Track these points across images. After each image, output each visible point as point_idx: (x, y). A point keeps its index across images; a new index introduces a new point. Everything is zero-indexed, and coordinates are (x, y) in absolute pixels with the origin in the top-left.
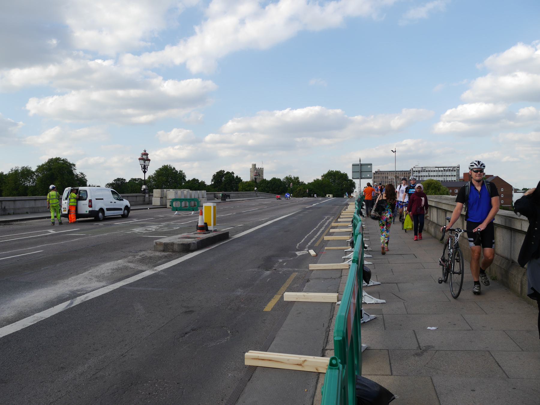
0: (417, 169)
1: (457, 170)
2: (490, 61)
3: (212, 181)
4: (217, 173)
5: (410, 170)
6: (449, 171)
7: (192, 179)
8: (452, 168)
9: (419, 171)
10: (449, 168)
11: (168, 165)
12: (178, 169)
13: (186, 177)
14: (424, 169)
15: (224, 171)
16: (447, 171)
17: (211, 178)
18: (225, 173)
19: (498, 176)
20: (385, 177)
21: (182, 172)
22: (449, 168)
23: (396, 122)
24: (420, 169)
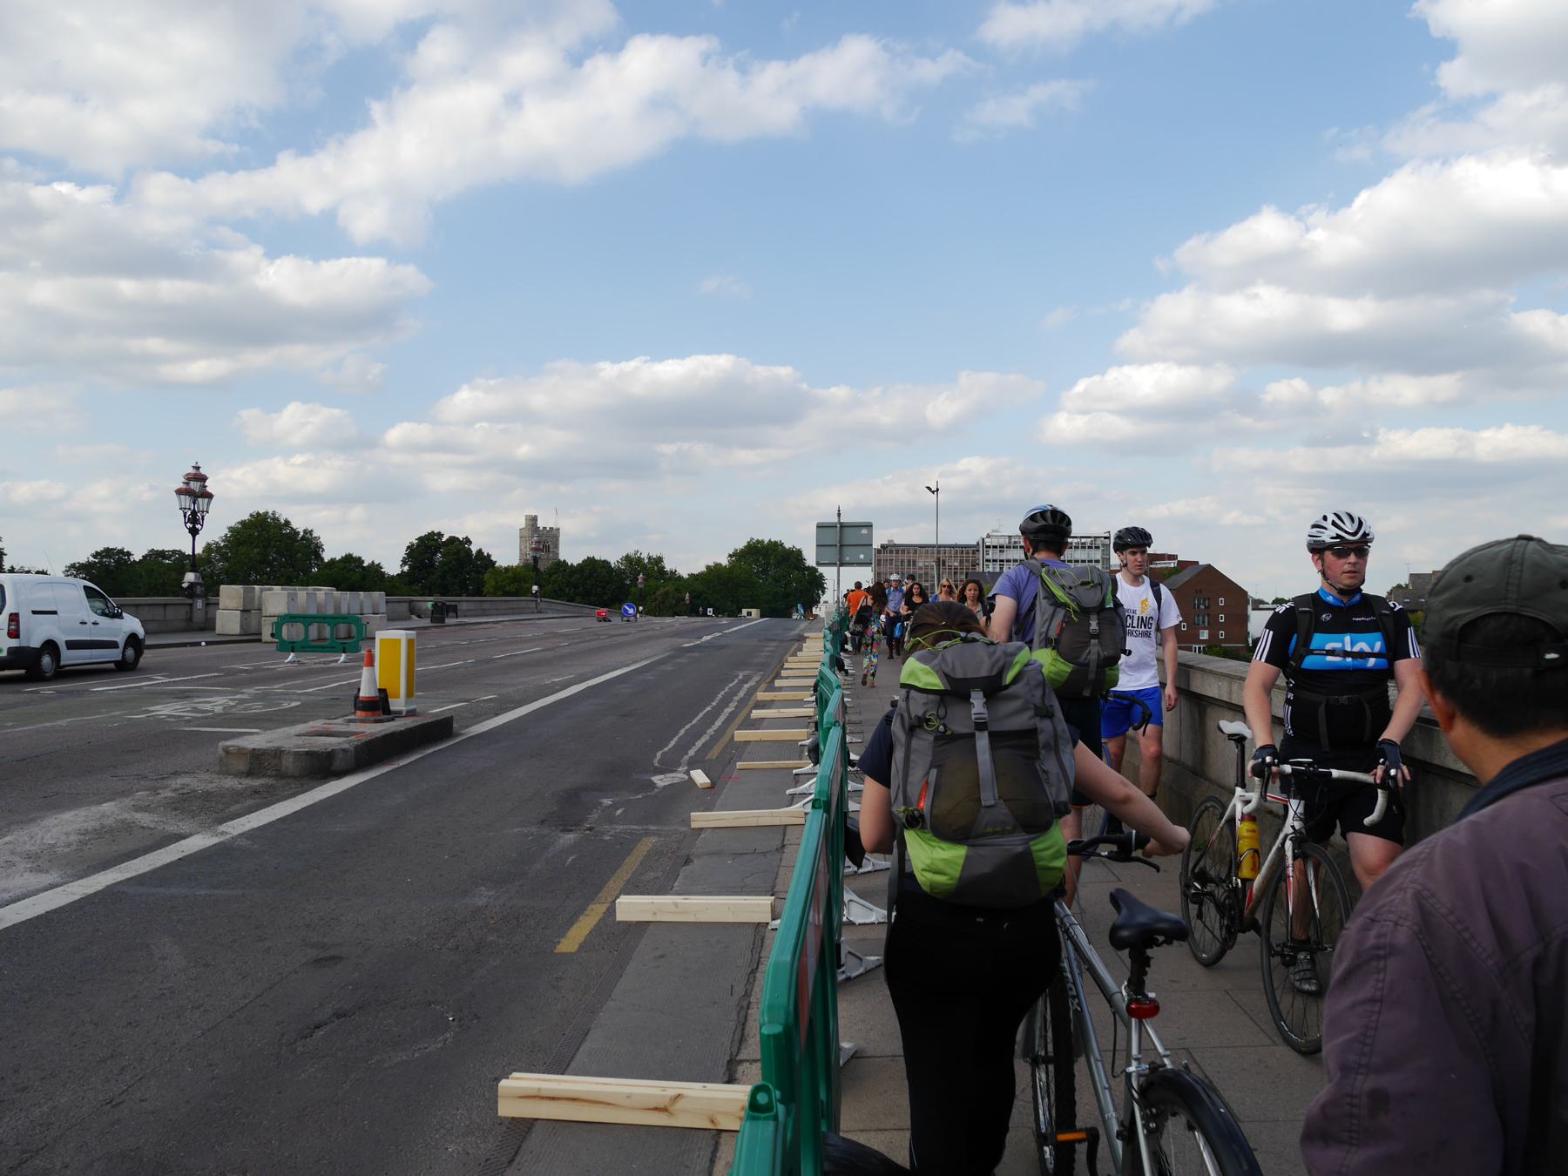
0: (995, 542)
1: (1103, 545)
2: (1190, 251)
3: (404, 562)
4: (420, 539)
5: (978, 543)
6: (1084, 548)
7: (344, 555)
8: (1089, 540)
9: (1002, 547)
10: (1083, 540)
11: (267, 513)
12: (299, 525)
13: (323, 550)
14: (1015, 542)
15: (440, 535)
16: (1077, 547)
17: (402, 553)
18: (444, 540)
19: (1210, 565)
20: (909, 561)
21: (311, 535)
22: (1083, 540)
23: (942, 408)
24: (1004, 542)
